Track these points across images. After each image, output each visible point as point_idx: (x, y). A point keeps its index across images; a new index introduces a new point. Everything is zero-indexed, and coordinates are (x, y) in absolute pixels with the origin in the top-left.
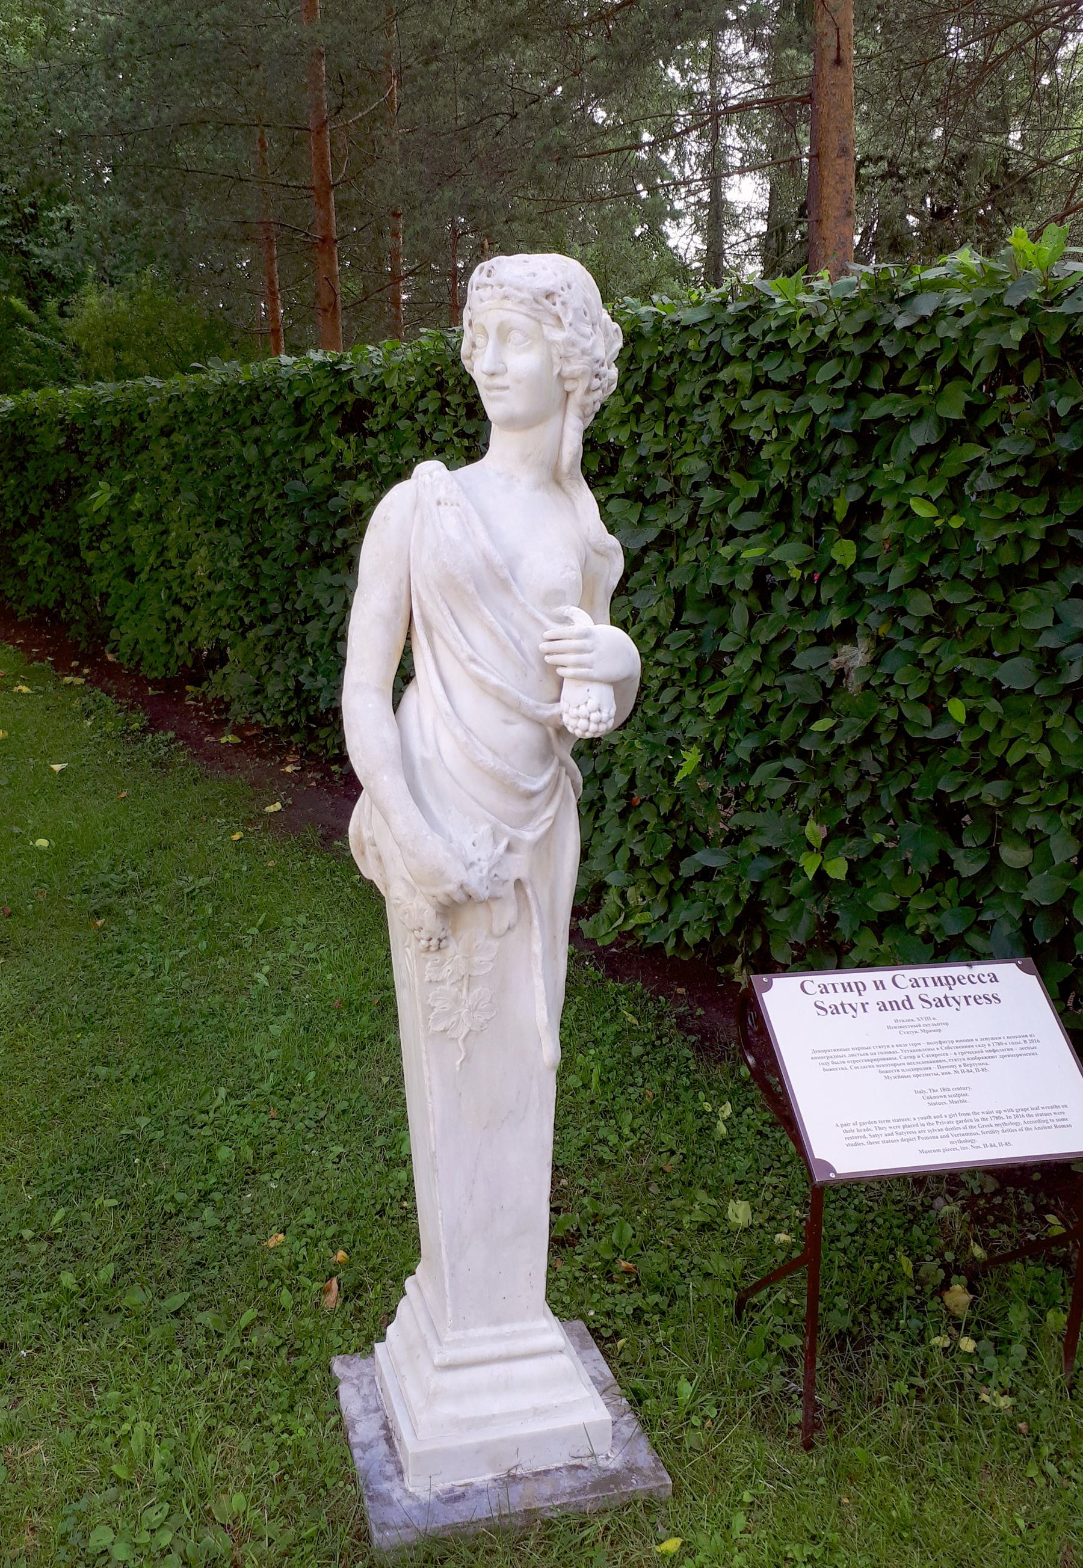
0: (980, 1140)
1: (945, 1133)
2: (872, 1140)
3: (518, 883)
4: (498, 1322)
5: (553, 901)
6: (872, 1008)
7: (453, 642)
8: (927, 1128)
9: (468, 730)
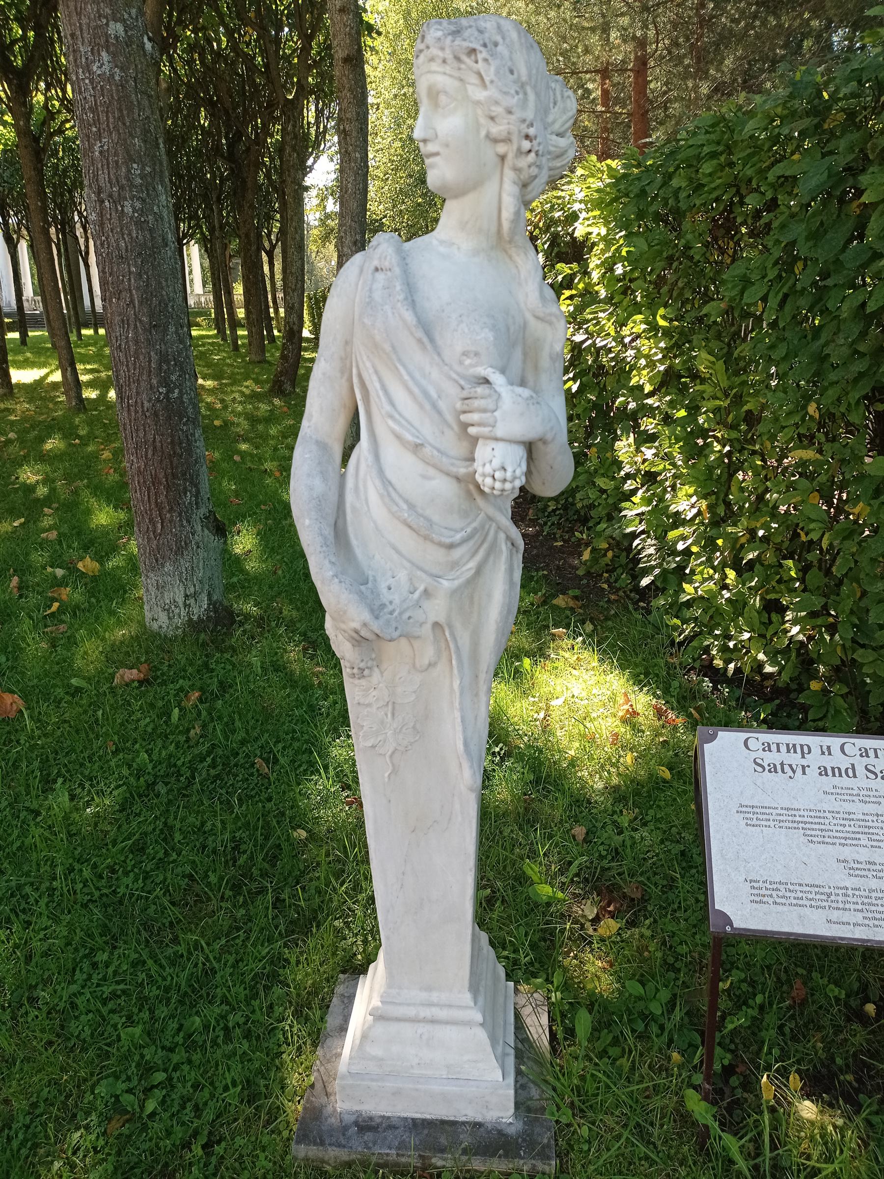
1: (860, 907)
3: (436, 625)
4: (429, 989)
6: (813, 772)
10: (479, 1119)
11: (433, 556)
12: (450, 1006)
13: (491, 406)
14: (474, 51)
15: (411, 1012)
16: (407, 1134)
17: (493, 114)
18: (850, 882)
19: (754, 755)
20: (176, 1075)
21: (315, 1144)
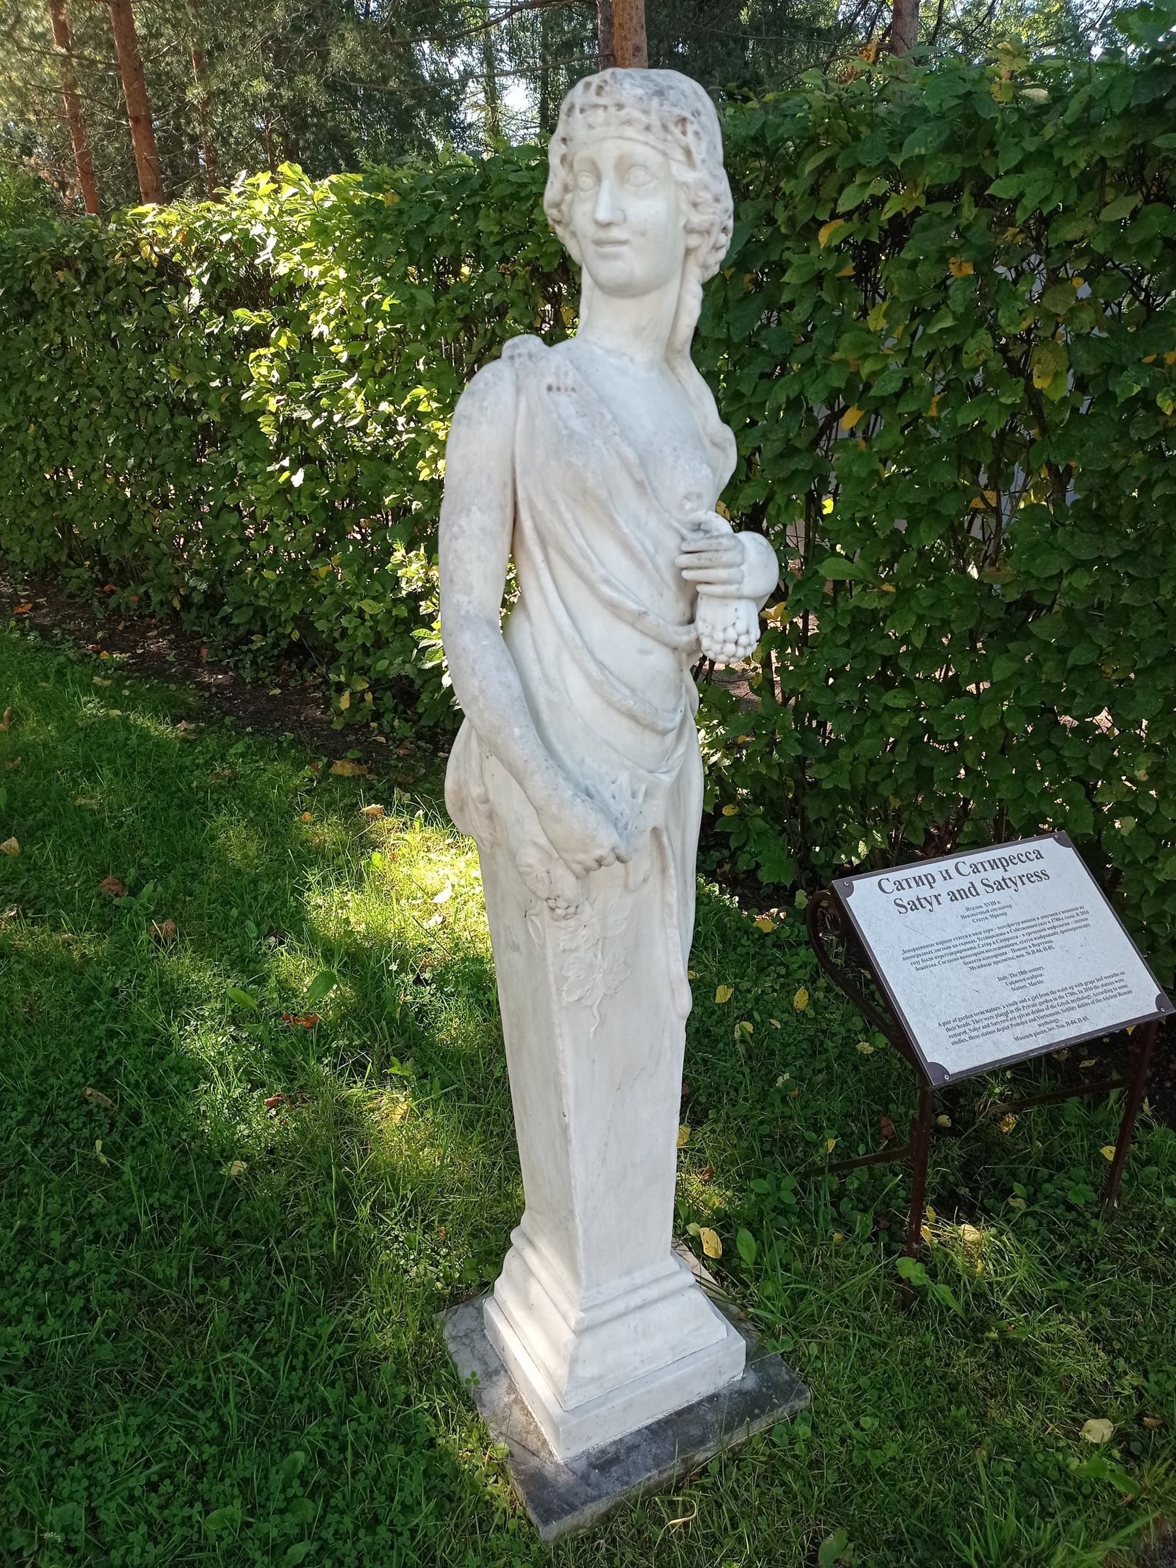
0: (1064, 1018)
2: (973, 1034)
4: (629, 1272)
5: (683, 844)
6: (944, 899)
7: (580, 560)
8: (1016, 1014)
9: (601, 665)
10: (711, 1390)
11: (650, 744)
12: (657, 1281)
13: (738, 560)
14: (684, 120)
15: (619, 1306)
16: (654, 1446)
17: (699, 200)
18: (1016, 996)
19: (892, 897)
20: (328, 1534)
21: (566, 1513)
